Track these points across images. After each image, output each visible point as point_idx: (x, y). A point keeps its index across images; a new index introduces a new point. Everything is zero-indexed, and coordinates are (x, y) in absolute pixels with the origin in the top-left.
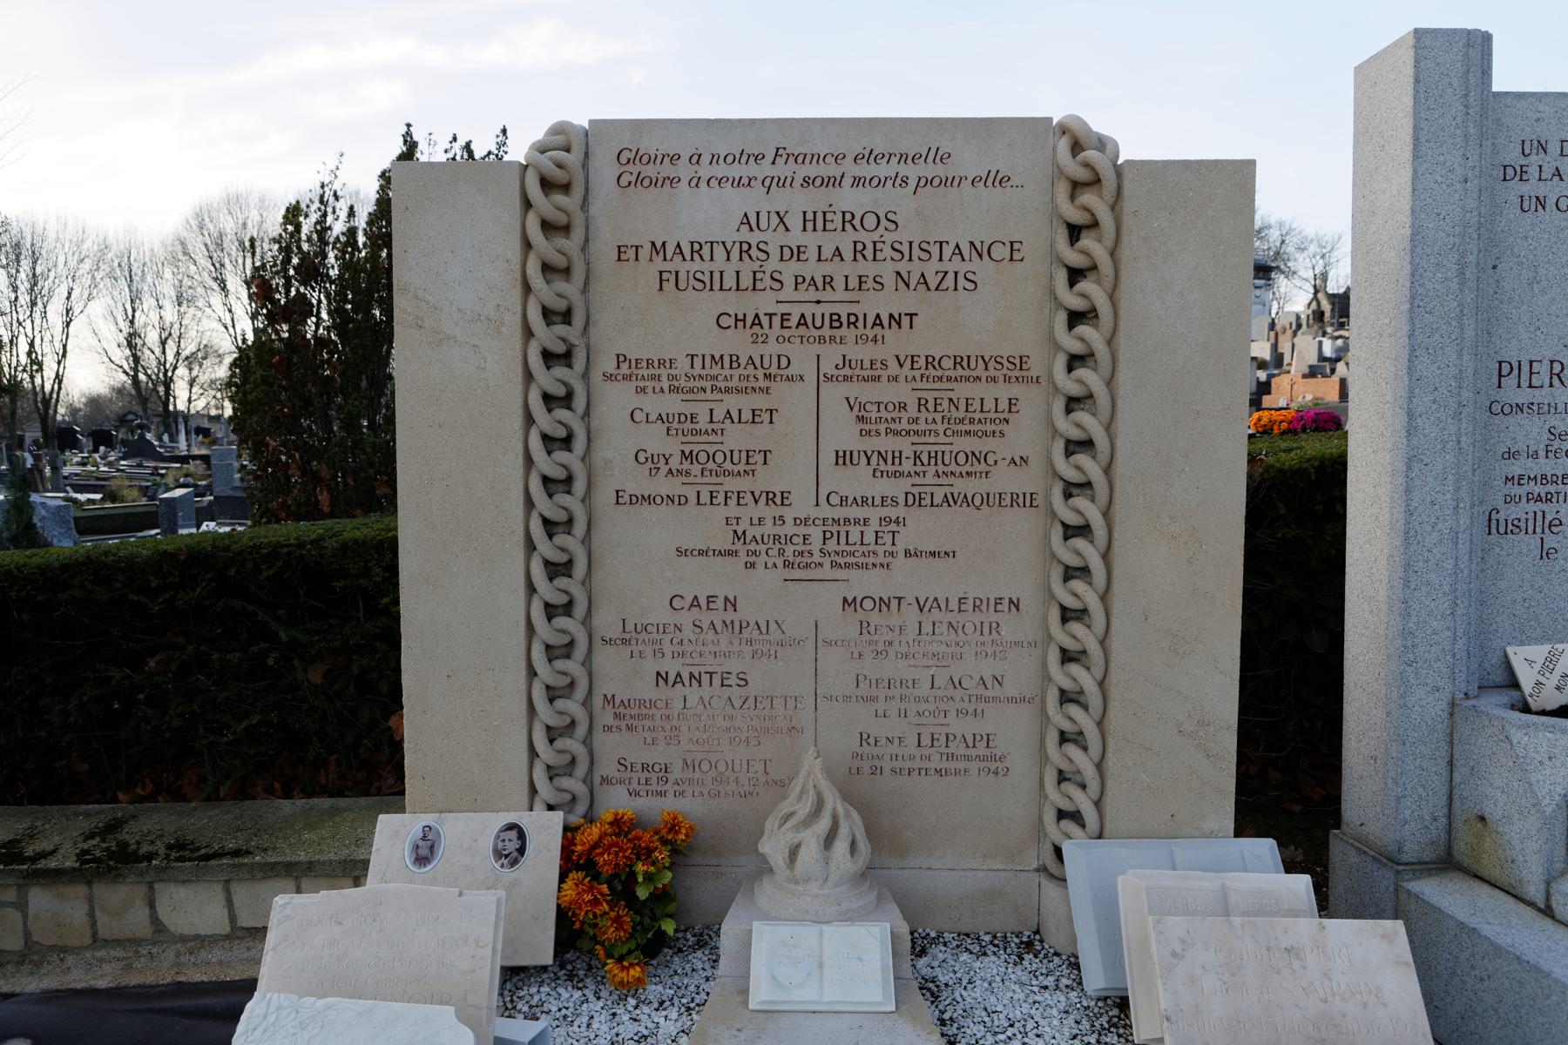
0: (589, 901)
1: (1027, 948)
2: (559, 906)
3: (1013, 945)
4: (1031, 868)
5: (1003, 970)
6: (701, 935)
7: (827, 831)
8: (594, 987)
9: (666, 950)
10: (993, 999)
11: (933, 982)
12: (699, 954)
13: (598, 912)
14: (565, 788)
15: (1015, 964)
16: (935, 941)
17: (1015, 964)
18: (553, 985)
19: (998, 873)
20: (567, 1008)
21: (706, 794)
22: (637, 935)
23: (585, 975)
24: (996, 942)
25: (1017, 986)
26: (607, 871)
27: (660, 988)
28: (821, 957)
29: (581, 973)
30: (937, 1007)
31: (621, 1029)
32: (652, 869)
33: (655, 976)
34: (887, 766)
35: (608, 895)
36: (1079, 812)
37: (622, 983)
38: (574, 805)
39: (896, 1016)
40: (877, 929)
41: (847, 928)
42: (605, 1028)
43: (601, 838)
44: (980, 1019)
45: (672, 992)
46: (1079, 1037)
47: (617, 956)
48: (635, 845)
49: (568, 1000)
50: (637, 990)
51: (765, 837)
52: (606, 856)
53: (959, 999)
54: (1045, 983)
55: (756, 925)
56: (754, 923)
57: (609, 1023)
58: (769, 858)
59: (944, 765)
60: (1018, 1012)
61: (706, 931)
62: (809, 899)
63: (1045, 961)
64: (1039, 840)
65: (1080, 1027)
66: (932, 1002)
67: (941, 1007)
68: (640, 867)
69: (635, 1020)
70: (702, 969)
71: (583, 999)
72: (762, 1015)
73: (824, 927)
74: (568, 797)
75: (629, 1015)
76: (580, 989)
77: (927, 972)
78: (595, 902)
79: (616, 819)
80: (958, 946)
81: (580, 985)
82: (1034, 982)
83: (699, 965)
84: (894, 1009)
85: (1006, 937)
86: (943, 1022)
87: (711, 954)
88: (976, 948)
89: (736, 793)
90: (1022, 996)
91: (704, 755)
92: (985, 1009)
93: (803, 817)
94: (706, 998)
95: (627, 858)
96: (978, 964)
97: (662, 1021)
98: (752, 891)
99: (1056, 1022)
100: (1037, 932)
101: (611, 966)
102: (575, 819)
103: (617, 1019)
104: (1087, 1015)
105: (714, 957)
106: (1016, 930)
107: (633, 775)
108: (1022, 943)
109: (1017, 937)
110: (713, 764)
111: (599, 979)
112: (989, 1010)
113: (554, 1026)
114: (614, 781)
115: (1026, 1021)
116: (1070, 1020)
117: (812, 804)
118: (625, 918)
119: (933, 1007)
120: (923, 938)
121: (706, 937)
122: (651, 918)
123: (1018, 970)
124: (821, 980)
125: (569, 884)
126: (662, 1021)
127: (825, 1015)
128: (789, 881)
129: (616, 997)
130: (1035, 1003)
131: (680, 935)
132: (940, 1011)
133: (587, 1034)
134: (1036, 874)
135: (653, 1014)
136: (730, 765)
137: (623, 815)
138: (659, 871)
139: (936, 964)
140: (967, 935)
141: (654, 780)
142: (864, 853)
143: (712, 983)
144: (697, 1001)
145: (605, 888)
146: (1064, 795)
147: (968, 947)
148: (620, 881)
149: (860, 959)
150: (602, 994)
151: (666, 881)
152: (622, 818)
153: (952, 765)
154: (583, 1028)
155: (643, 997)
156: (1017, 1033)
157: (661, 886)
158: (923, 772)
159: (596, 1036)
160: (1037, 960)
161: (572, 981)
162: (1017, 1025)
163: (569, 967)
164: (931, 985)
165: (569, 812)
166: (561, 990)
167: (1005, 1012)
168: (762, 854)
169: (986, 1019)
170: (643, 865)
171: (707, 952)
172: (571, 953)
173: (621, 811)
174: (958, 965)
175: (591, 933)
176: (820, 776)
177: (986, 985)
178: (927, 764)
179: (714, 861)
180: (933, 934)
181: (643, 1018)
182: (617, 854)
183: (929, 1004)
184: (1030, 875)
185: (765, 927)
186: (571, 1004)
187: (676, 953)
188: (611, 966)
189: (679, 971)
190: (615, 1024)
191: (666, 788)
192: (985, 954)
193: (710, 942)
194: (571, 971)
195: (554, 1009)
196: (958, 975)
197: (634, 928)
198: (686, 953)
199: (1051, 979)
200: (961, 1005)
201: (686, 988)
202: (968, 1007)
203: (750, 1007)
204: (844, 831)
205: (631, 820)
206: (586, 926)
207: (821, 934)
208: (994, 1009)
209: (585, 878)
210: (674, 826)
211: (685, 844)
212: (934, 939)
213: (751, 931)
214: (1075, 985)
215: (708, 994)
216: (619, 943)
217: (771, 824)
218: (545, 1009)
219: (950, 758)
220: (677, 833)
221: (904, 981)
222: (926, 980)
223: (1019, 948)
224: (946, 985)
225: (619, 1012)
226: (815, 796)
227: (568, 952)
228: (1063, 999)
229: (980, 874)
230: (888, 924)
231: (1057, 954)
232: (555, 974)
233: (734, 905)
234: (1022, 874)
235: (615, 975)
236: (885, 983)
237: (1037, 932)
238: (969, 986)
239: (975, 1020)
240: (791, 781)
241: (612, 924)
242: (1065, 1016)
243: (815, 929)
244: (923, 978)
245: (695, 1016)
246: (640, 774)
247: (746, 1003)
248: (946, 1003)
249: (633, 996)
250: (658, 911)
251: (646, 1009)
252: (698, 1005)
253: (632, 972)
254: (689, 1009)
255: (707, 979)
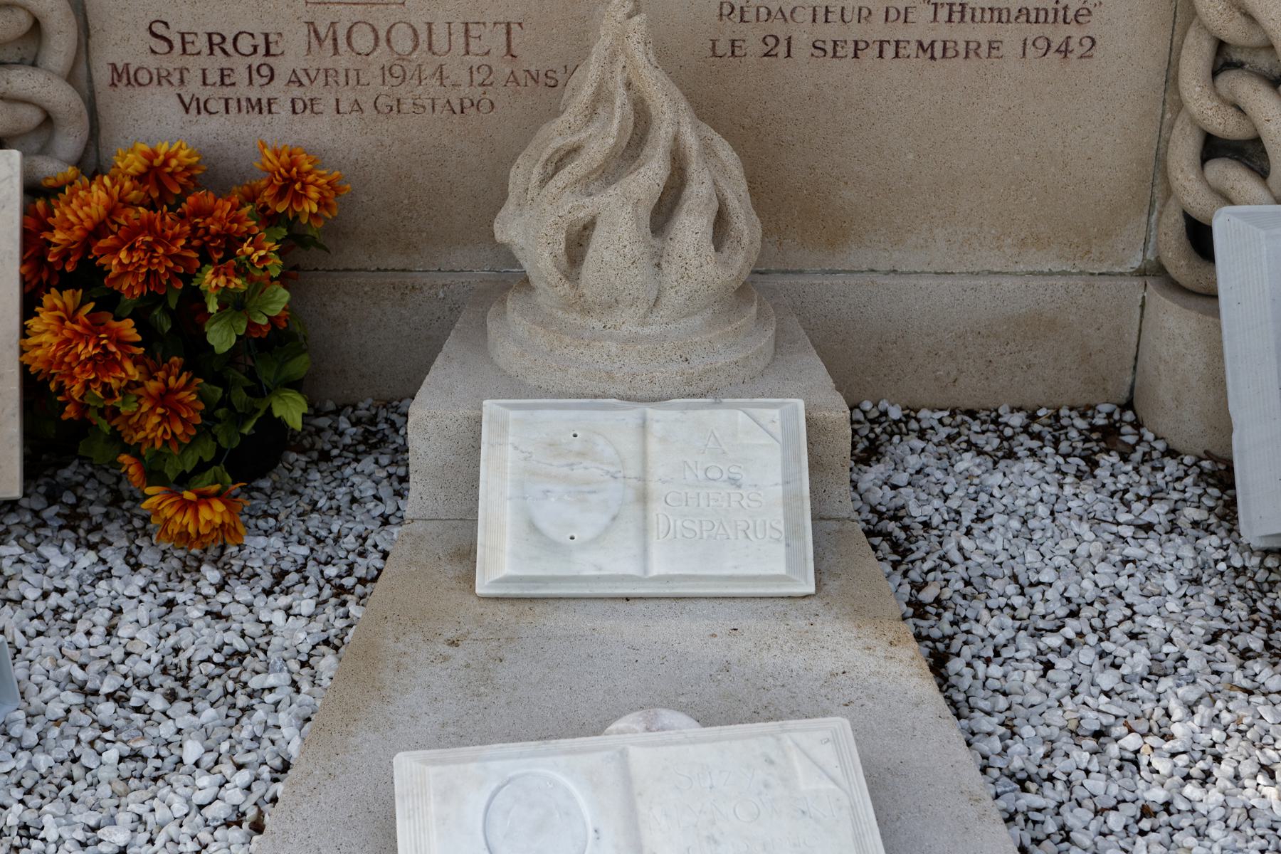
0: (90, 359)
1: (1103, 439)
2: (24, 368)
3: (1073, 434)
4: (1127, 268)
5: (1053, 489)
6: (373, 421)
7: (657, 191)
8: (125, 543)
9: (293, 456)
10: (1031, 557)
11: (895, 518)
12: (367, 464)
13: (114, 384)
14: (22, 94)
15: (1080, 476)
16: (898, 428)
17: (1080, 476)
18: (31, 539)
19: (1051, 281)
20: (62, 592)
21: (368, 107)
22: (218, 428)
23: (106, 515)
24: (1036, 428)
25: (1085, 526)
26: (131, 288)
27: (276, 542)
28: (643, 479)
29: (97, 511)
30: (905, 574)
31: (185, 637)
32: (238, 283)
33: (265, 515)
34: (803, 36)
35: (137, 344)
36: (1257, 140)
37: (184, 538)
38: (51, 137)
39: (815, 604)
40: (776, 413)
41: (705, 414)
42: (146, 636)
43: (111, 211)
44: (1003, 601)
45: (304, 551)
46: (1226, 637)
47: (171, 476)
48: (195, 228)
49: (64, 574)
50: (223, 548)
51: (510, 206)
52: (123, 255)
53: (955, 556)
54: (1148, 517)
55: (490, 407)
56: (487, 403)
57: (156, 625)
58: (519, 255)
59: (943, 32)
60: (1087, 584)
61: (383, 413)
62: (613, 348)
63: (1146, 469)
64: (1152, 205)
65: (1226, 613)
66: (895, 565)
67: (914, 575)
68: (209, 280)
69: (218, 616)
70: (375, 497)
71: (98, 569)
72: (506, 607)
73: (653, 412)
74: (33, 117)
75: (203, 607)
76: (92, 547)
77: (881, 496)
78: (104, 362)
79: (150, 168)
80: (950, 438)
81: (94, 538)
82: (1123, 517)
83: (367, 489)
84: (811, 589)
85: (1057, 417)
86: (919, 609)
87: (392, 463)
88: (991, 442)
89: (440, 103)
90: (1097, 548)
91: (358, 13)
92: (1014, 578)
93: (599, 158)
94: (379, 564)
95: (175, 258)
96: (996, 479)
97: (278, 618)
98: (483, 327)
99: (1173, 605)
100: (1128, 405)
101: (155, 500)
102: (52, 168)
103: (177, 614)
104: (1240, 587)
105: (401, 471)
106: (1081, 401)
107: (188, 61)
108: (1093, 428)
109: (1083, 416)
110: (382, 34)
111: (137, 523)
112: (1022, 579)
113: (31, 631)
114: (143, 77)
115: (1105, 602)
116: (1205, 601)
117: (622, 128)
118: (183, 395)
119: (897, 577)
120: (872, 421)
121: (382, 426)
122: (249, 391)
123: (1086, 488)
124: (644, 531)
125: (43, 320)
126: (278, 618)
127: (651, 604)
128: (568, 306)
129: (175, 563)
130: (1125, 562)
131: (324, 422)
132: (913, 584)
133: (104, 650)
134: (1137, 282)
135: (260, 602)
136: (423, 36)
137: (168, 157)
138: (257, 287)
139: (901, 478)
140: (972, 414)
141: (241, 75)
142: (746, 240)
143: (395, 530)
144: (360, 572)
145: (128, 328)
146: (1224, 101)
147: (974, 439)
148: (167, 310)
149: (735, 482)
150: (142, 559)
151: (276, 309)
152: (166, 163)
153: (960, 33)
154: (96, 639)
155: (237, 565)
156: (1087, 629)
157: (263, 321)
158: (889, 51)
159: (128, 654)
160: (1129, 468)
161: (74, 529)
162: (1086, 612)
163: (69, 498)
164: (892, 526)
165: (44, 151)
166: (49, 551)
167: (1060, 585)
168: (503, 245)
169: (1018, 601)
170: (216, 274)
171: (385, 460)
172: (72, 468)
173: (163, 149)
174: (951, 480)
175: (106, 428)
176: (640, 58)
177: (1015, 524)
178: (899, 31)
179: (395, 261)
180: (895, 413)
181: (236, 611)
182: (151, 249)
183: (889, 569)
184: (1124, 283)
185: (513, 414)
186: (71, 583)
187: (315, 463)
188: (155, 500)
189: (322, 503)
190: (171, 627)
191: (269, 92)
192: (1011, 455)
193: (392, 436)
194: (74, 507)
195: (32, 594)
196: (954, 503)
197: (208, 415)
198: (337, 462)
199: (1160, 508)
200: (960, 569)
201: (336, 540)
202: (975, 573)
203: (477, 591)
204: (699, 190)
205: (188, 168)
206: (92, 415)
207: (643, 426)
208: (1034, 579)
209: (83, 304)
210: (289, 182)
211: (320, 225)
212: (896, 422)
213: (478, 421)
214: (1213, 520)
215: (385, 555)
216: (174, 449)
217: (523, 174)
218: (12, 595)
219: (956, 17)
220: (299, 197)
221: (834, 526)
222: (881, 516)
223: (1086, 440)
224: (926, 525)
225: (180, 598)
226: (628, 108)
227: (65, 465)
228: (1187, 552)
229: (1007, 283)
230: (800, 404)
231: (1171, 453)
232: (36, 513)
233: (439, 360)
234: (1106, 282)
235: (167, 521)
236: (792, 533)
237: (1128, 405)
238: (978, 528)
239: (991, 603)
240: (570, 71)
241: (153, 409)
242: (1192, 590)
243: (629, 415)
244: (873, 510)
245: (353, 609)
246: (204, 61)
247: (470, 579)
248: (926, 566)
249: (215, 563)
250: (267, 375)
251: (243, 592)
252: (362, 581)
253: (205, 513)
254: (340, 590)
255: (385, 521)
